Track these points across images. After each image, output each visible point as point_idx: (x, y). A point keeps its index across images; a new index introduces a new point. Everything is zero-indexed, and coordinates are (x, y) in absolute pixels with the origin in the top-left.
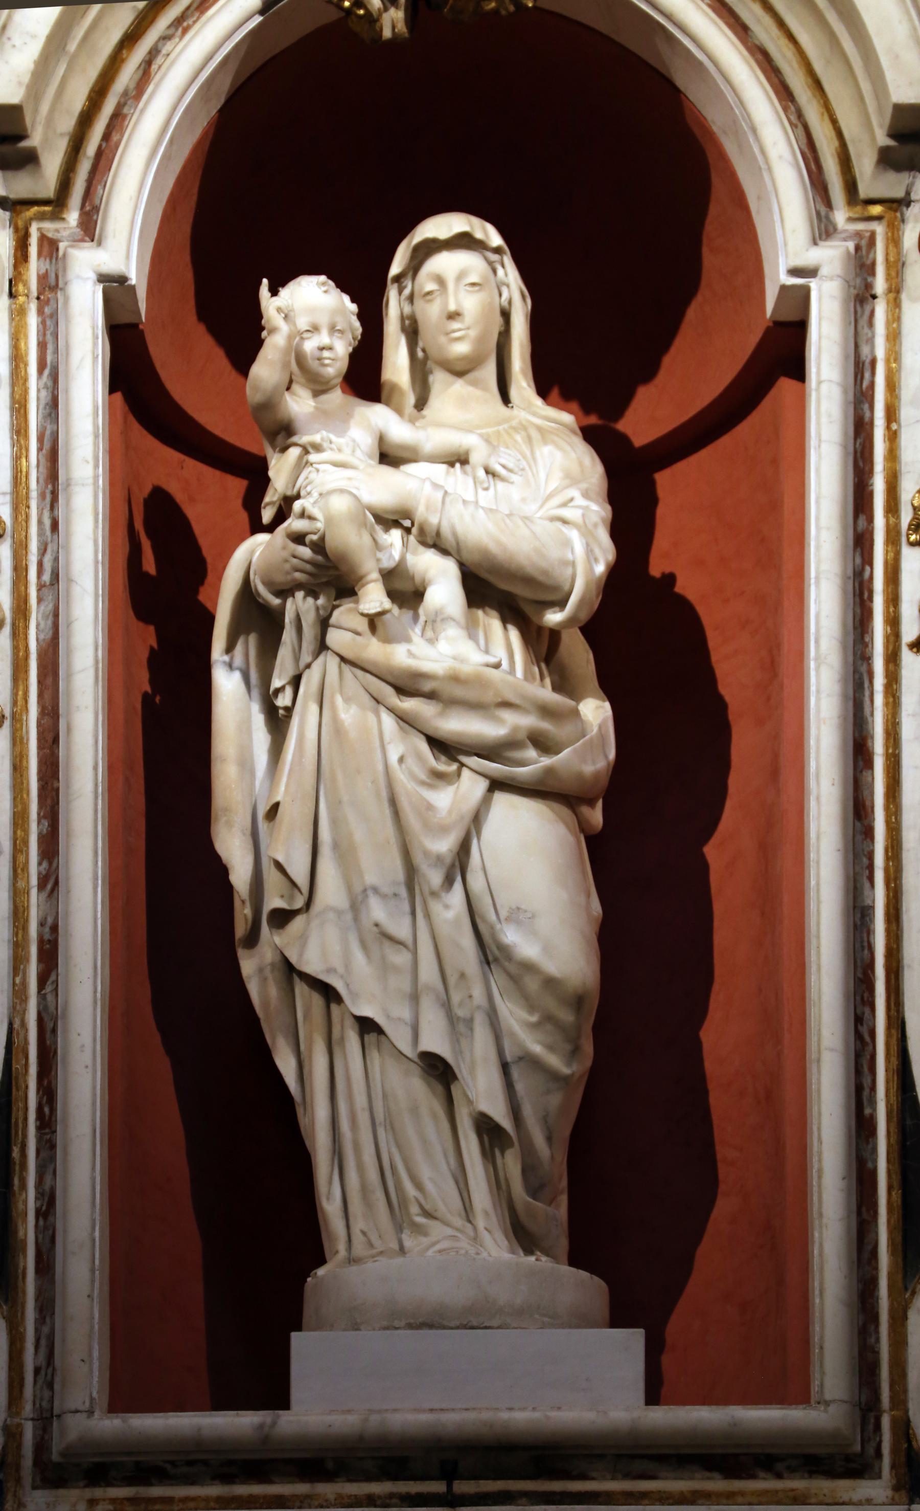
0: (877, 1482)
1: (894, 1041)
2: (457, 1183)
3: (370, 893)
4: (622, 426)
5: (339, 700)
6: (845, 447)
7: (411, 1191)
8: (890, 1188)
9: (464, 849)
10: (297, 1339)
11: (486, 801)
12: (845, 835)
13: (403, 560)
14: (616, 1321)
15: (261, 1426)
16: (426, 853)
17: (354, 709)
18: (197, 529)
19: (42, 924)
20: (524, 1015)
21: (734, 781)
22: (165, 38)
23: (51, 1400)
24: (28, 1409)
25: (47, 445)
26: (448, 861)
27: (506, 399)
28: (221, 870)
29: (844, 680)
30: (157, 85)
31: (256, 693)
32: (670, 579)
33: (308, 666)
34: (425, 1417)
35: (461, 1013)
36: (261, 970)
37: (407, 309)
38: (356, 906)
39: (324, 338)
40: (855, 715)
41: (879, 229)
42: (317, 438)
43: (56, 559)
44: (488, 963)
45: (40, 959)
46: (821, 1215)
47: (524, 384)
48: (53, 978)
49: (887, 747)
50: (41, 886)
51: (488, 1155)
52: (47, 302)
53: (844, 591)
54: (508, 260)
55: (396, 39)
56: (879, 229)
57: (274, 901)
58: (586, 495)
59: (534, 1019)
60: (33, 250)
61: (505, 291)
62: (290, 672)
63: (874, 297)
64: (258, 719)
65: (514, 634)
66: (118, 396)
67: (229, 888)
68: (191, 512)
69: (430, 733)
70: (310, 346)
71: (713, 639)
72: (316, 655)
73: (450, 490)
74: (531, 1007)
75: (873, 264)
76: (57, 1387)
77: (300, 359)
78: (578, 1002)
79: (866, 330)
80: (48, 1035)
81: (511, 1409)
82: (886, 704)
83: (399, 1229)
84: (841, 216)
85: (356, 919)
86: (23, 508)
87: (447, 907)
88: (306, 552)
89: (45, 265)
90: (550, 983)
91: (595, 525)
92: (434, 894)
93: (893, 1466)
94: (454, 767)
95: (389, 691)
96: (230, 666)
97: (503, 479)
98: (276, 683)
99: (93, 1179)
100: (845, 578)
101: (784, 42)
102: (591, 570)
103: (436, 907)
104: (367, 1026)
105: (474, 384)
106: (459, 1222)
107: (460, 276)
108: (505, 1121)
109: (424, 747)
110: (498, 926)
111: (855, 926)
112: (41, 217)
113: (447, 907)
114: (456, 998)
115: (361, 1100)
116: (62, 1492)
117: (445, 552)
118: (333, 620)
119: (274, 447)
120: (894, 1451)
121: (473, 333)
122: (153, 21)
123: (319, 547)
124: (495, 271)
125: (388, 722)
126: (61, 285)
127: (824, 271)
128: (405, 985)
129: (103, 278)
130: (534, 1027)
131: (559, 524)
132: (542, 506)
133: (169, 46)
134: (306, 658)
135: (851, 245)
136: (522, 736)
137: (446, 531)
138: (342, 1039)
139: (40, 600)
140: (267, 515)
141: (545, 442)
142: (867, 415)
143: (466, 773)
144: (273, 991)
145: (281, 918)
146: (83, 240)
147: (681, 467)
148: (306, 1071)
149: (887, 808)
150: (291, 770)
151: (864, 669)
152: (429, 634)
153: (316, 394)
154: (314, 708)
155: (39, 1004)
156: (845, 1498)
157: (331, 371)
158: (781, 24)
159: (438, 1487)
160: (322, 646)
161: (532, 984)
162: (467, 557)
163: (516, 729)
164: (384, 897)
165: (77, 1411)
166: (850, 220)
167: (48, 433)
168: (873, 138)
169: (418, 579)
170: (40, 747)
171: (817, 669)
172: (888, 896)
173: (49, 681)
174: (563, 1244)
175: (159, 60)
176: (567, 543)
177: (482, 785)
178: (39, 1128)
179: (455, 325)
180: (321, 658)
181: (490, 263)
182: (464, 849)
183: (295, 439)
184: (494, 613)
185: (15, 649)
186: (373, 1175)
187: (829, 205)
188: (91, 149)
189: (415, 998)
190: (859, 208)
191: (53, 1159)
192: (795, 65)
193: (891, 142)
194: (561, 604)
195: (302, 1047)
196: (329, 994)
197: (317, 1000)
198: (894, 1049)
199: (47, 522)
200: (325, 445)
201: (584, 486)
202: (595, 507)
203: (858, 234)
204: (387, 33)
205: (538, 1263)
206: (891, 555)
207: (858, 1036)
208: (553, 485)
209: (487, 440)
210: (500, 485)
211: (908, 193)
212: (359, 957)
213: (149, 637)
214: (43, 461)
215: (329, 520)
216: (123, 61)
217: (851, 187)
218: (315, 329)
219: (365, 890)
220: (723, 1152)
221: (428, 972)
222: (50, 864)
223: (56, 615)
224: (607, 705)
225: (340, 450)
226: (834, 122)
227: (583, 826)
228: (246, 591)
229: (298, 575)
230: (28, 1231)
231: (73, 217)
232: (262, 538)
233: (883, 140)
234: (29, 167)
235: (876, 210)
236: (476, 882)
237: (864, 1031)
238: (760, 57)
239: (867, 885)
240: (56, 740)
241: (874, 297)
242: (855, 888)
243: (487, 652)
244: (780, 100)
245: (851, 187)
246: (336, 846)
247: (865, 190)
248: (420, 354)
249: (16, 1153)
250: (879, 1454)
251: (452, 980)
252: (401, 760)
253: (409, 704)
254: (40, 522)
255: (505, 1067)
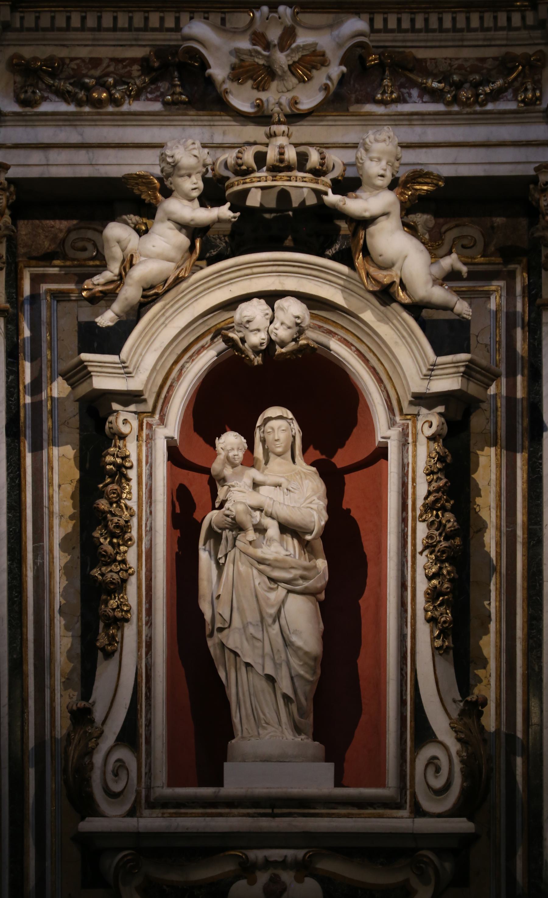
0: (405, 811)
1: (413, 676)
2: (276, 713)
3: (249, 624)
4: (333, 460)
5: (240, 564)
6: (399, 492)
7: (262, 716)
8: (411, 721)
9: (279, 611)
10: (227, 766)
11: (286, 596)
12: (398, 613)
13: (260, 521)
14: (327, 760)
15: (215, 792)
16: (267, 613)
17: (244, 567)
18: (193, 494)
19: (146, 636)
20: (297, 661)
21: (368, 581)
22: (187, 362)
23: (150, 783)
24: (143, 785)
25: (148, 487)
26: (274, 615)
27: (294, 462)
28: (202, 615)
29: (398, 565)
30: (184, 377)
31: (213, 558)
32: (349, 511)
33: (230, 551)
34: (265, 790)
35: (278, 662)
36: (214, 645)
37: (262, 435)
38: (245, 627)
39: (235, 452)
40: (402, 575)
41: (410, 423)
42: (233, 483)
43: (151, 523)
44: (287, 646)
45: (146, 647)
46: (389, 730)
47: (300, 459)
48: (150, 653)
49: (412, 584)
50: (146, 624)
51: (286, 705)
52: (149, 443)
53: (398, 537)
54: (295, 422)
55: (258, 366)
56: (410, 423)
57: (218, 625)
58: (319, 498)
59: (301, 663)
60: (144, 427)
61: (293, 430)
62: (224, 553)
63: (408, 443)
64: (214, 566)
65: (296, 541)
66: (169, 462)
67: (204, 620)
68: (191, 489)
69: (268, 576)
70: (231, 454)
71: (362, 533)
72: (232, 548)
73: (275, 500)
74: (300, 660)
75: (408, 433)
76: (152, 779)
77: (228, 458)
78: (315, 659)
79: (406, 454)
80: (149, 671)
81: (292, 788)
82: (412, 571)
83: (258, 727)
84: (398, 418)
85: (245, 631)
86: (140, 507)
87: (273, 629)
88: (229, 520)
89: (148, 432)
90: (306, 653)
91: (321, 510)
92: (270, 626)
93: (410, 806)
94: (276, 586)
95: (256, 562)
96: (205, 550)
97: (292, 492)
98: (219, 556)
99: (163, 716)
100: (398, 533)
101: (380, 365)
102: (320, 524)
103: (270, 629)
104: (248, 665)
105: (284, 458)
106: (277, 726)
107: (279, 428)
108: (291, 695)
109: (267, 580)
110: (290, 635)
111: (401, 641)
112: (147, 417)
113: (273, 629)
114: (276, 657)
115: (246, 688)
116: (154, 810)
117: (273, 518)
118: (238, 538)
119: (220, 484)
120: (410, 801)
121: (283, 445)
122: (183, 357)
123: (234, 519)
124: (290, 425)
125: (255, 572)
126: (153, 438)
127: (392, 438)
128: (260, 652)
129: (166, 438)
130: (301, 666)
131: (309, 509)
132: (305, 501)
133: (188, 365)
134: (229, 549)
135: (400, 429)
136: (297, 577)
137: (274, 513)
138: (240, 668)
139: (146, 535)
140: (217, 505)
141: (306, 478)
142: (406, 480)
143: (280, 588)
144: (218, 652)
145: (221, 630)
146: (160, 425)
147: (353, 474)
148: (228, 676)
149: (411, 603)
150: (224, 584)
151: (405, 560)
152: (268, 543)
153: (233, 467)
154: (232, 565)
155: (146, 661)
156: (395, 816)
157: (237, 462)
158: (379, 360)
159: (269, 811)
160: (234, 546)
161: (300, 653)
162: (281, 521)
163: (295, 575)
164: (253, 625)
165: (158, 787)
166: (401, 420)
167: (149, 484)
168: (407, 397)
169: (265, 526)
170: (146, 581)
171: (390, 561)
172: (411, 631)
173: (149, 560)
174: (311, 730)
175: (185, 369)
176: (312, 516)
177: (285, 592)
178: (146, 699)
179: (277, 443)
180: (234, 549)
181: (289, 423)
182: (279, 611)
183: (226, 484)
184: (289, 535)
185: (138, 551)
186: (250, 711)
187: (394, 415)
188: (163, 395)
189: (263, 656)
190: (403, 416)
191: (150, 709)
192: (383, 372)
193: (413, 399)
194: (311, 533)
195: (227, 669)
196: (236, 654)
197: (232, 656)
198: (413, 678)
199: (148, 511)
200: (236, 485)
201: (318, 495)
202: (322, 503)
203: (403, 424)
204: (256, 363)
205: (302, 742)
206: (414, 525)
207: (402, 674)
208: (308, 494)
209: (287, 480)
210: (292, 494)
211: (419, 412)
212: (245, 643)
213: (178, 533)
214: (147, 492)
215: (237, 512)
216: (173, 369)
217: (401, 410)
218: (233, 449)
219: (247, 623)
220: (364, 700)
221: (268, 649)
222: (149, 618)
223: (151, 541)
224: (326, 561)
225: (240, 487)
226: (396, 390)
227: (318, 600)
228: (210, 527)
229: (227, 526)
230: (143, 731)
231: (157, 416)
232: (215, 512)
233: (410, 398)
234: (144, 403)
235: (409, 417)
236: (283, 622)
237: (404, 673)
238: (372, 370)
239: (405, 627)
240: (151, 579)
241: (408, 443)
242: (401, 628)
243: (287, 550)
244: (378, 383)
245: (401, 410)
246: (238, 608)
247: (405, 411)
248: (266, 447)
249: (139, 707)
250: (406, 802)
251: (275, 652)
252: (259, 584)
253: (262, 567)
254: (146, 511)
255: (292, 678)
